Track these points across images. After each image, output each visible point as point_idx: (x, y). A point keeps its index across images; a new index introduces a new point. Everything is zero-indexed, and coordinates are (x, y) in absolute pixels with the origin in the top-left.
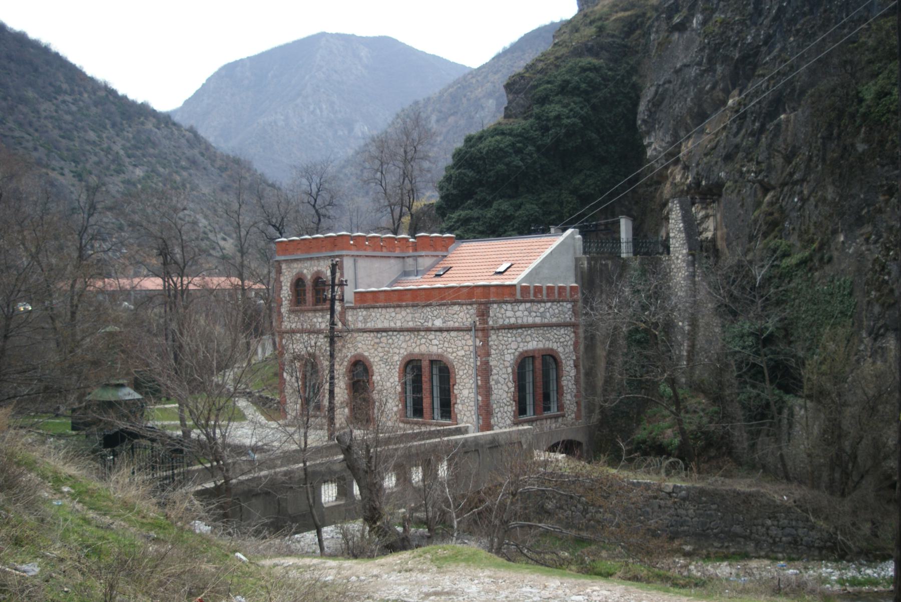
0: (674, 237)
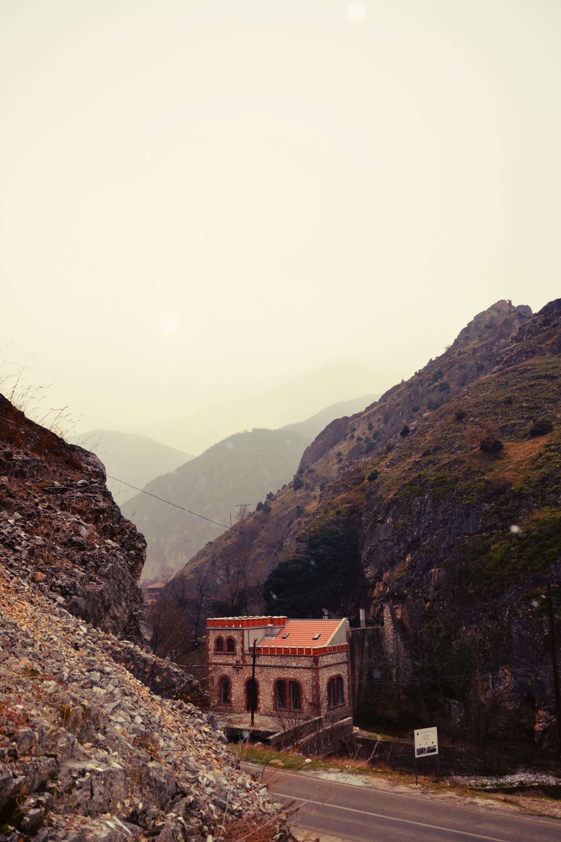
0: (386, 620)
